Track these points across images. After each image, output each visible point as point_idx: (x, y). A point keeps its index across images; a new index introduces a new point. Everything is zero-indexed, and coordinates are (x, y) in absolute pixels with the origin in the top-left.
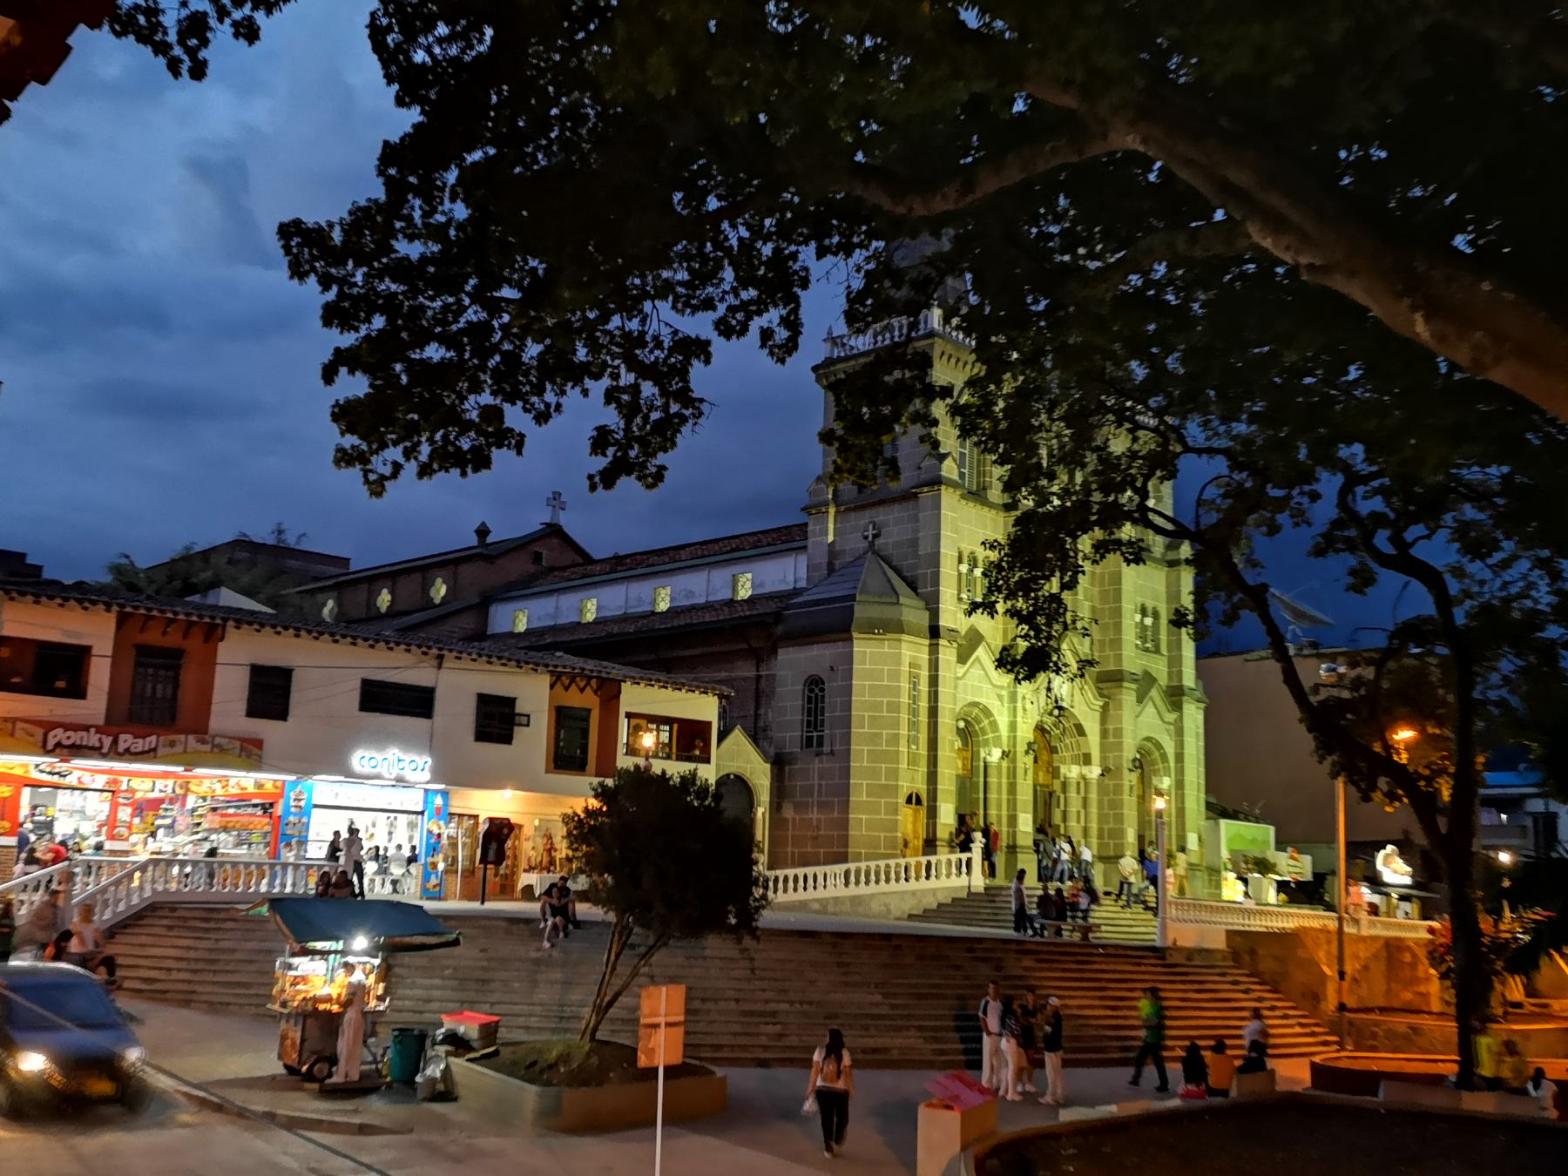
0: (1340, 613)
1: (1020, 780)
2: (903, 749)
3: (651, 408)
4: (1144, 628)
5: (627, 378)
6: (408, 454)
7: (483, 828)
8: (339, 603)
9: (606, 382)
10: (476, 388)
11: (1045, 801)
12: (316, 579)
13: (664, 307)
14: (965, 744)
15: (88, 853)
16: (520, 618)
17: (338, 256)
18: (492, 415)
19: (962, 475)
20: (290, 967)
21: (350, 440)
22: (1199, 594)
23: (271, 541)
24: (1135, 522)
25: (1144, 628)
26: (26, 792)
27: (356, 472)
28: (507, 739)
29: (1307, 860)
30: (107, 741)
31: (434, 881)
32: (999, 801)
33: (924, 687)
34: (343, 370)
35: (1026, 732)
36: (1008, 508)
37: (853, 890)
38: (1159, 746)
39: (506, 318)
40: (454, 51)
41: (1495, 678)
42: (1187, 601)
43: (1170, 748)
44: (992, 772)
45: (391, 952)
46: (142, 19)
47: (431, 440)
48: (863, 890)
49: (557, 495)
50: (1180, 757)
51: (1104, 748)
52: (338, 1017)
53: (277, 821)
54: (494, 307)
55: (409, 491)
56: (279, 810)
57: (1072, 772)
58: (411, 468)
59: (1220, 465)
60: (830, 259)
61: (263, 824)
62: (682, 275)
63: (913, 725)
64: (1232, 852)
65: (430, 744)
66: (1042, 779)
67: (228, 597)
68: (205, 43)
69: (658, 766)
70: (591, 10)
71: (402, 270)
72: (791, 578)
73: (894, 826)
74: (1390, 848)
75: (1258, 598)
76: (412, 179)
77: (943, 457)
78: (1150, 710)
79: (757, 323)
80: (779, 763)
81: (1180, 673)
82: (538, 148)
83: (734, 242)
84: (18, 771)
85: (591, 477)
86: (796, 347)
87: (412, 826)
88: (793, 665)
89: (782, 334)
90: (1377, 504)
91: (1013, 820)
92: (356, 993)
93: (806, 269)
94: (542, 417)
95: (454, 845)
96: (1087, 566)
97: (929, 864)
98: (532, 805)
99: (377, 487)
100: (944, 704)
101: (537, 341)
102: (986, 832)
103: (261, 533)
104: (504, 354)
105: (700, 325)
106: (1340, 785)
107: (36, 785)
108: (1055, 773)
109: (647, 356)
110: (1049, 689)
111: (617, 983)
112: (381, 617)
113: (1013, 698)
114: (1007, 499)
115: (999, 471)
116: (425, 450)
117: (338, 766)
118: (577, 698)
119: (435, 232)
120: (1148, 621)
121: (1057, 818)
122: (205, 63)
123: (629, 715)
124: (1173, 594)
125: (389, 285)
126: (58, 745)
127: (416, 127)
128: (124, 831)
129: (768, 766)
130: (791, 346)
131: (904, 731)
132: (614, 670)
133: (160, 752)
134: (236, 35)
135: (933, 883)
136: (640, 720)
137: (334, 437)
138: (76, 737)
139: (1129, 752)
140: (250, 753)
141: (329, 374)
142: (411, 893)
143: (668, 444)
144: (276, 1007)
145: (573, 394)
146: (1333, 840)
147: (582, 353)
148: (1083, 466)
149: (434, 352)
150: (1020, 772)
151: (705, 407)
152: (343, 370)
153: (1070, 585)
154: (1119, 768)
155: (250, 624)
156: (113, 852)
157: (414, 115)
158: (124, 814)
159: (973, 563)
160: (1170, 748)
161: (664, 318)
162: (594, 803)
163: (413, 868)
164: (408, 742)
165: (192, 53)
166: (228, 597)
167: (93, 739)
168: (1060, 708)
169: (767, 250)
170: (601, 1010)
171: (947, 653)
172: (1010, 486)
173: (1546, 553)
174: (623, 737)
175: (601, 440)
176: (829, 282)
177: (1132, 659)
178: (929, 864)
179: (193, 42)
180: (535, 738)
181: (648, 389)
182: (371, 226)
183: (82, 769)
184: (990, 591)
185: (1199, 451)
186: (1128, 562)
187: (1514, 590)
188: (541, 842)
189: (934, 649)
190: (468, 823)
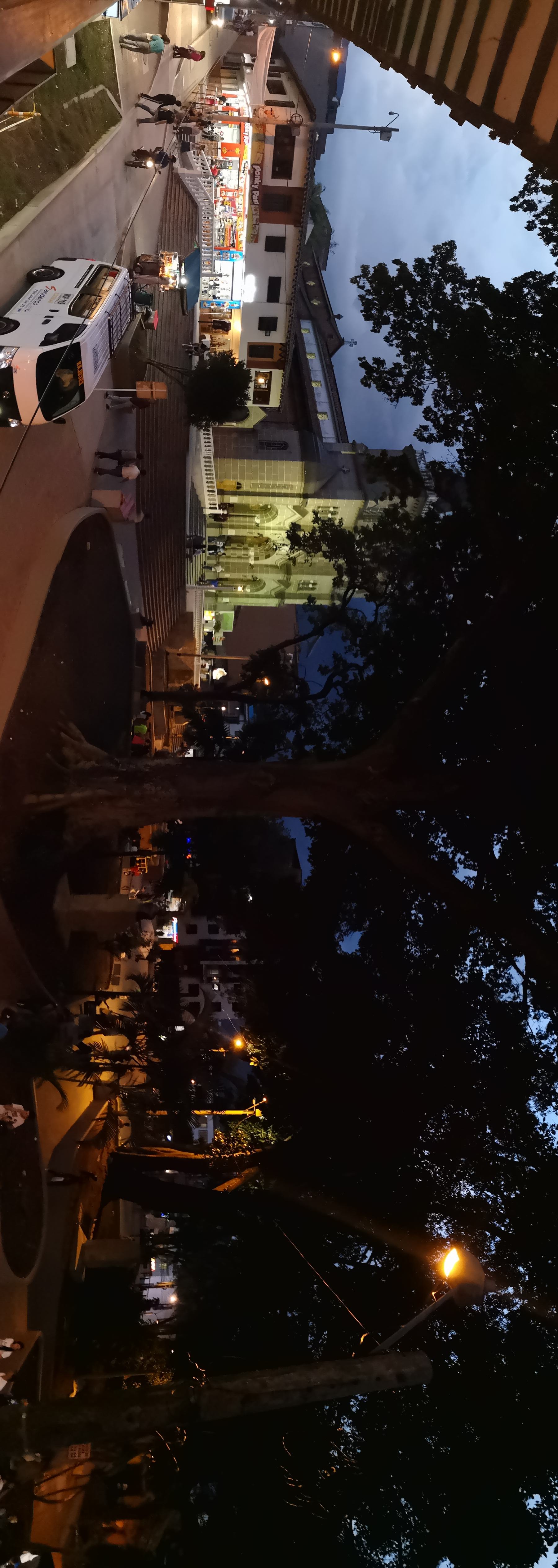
0: (312, 663)
1: (247, 530)
2: (259, 482)
3: (393, 382)
4: (308, 583)
5: (405, 372)
6: (368, 292)
7: (227, 321)
8: (309, 267)
9: (403, 363)
10: (395, 315)
11: (239, 541)
12: (318, 258)
13: (435, 386)
14: (262, 508)
15: (215, 182)
16: (306, 327)
17: (443, 262)
18: (386, 321)
19: (369, 509)
20: (175, 257)
21: (372, 271)
22: (321, 607)
23: (332, 241)
24: (349, 583)
25: (308, 583)
26: (238, 159)
27: (360, 273)
28: (260, 328)
29: (220, 644)
30: (256, 187)
31: (207, 305)
32: (239, 521)
33: (283, 491)
34: (398, 267)
35: (267, 534)
36: (355, 528)
37: (202, 460)
38: (262, 588)
39: (425, 325)
40: (530, 302)
41: (287, 711)
42: (319, 602)
43: (261, 592)
44: (251, 519)
45: (182, 291)
46: (533, 186)
47: (374, 299)
48: (203, 464)
49: (356, 343)
50: (258, 596)
51: (261, 566)
52: (157, 275)
53: (228, 249)
54: (429, 320)
55: (354, 292)
56: (232, 250)
57: (252, 553)
58: (363, 293)
59: (371, 619)
60: (457, 455)
61: (227, 243)
62: (448, 393)
63: (268, 486)
64: (222, 615)
65: (257, 302)
66: (249, 539)
67: (310, 228)
68: (525, 210)
69: (251, 385)
70: (555, 355)
71: (440, 287)
72: (326, 436)
73: (228, 477)
74: (226, 673)
75: (318, 631)
76: (476, 289)
77: (377, 502)
78: (275, 585)
79: (429, 424)
80: (253, 431)
81: (289, 598)
82: (495, 335)
83: (462, 414)
84: (245, 155)
85: (364, 358)
86: (421, 440)
87: (227, 297)
88: (292, 436)
89: (426, 435)
90: (351, 677)
91: (232, 527)
92: (165, 281)
93: (453, 445)
94: (387, 339)
95: (220, 311)
96: (333, 562)
97: (213, 491)
98: (236, 337)
99: (354, 281)
100: (277, 499)
101: (417, 336)
102: (227, 515)
103: (334, 238)
104: (410, 324)
105: (428, 401)
106: (247, 658)
107: (240, 162)
108: (251, 545)
109: (415, 380)
110: (284, 545)
111: (169, 372)
112: (305, 281)
113: (280, 529)
114: (359, 528)
115: (371, 525)
116: (370, 297)
117: (248, 270)
118: (276, 353)
119: (455, 297)
120: (310, 586)
121: (234, 545)
122: (517, 210)
123: (271, 373)
124: (321, 597)
125: (433, 283)
126: (255, 170)
127: (497, 290)
128: (224, 194)
129: (252, 427)
130: (421, 438)
131: (265, 482)
132: (288, 368)
133: (253, 206)
134: (529, 222)
135: (206, 493)
136: (269, 377)
137: (372, 264)
138: (257, 175)
139: (259, 576)
140: (253, 238)
141: (397, 262)
142: (202, 297)
143: (379, 389)
144: (161, 253)
145: (397, 351)
146: (229, 654)
147: (414, 354)
148: (372, 562)
149: (408, 299)
150: (251, 531)
151: (395, 403)
152: (398, 267)
153: (325, 555)
154: (253, 572)
155: (309, 164)
156: (216, 191)
157: (502, 289)
158: (230, 194)
159: (334, 513)
160: (261, 592)
161: (431, 386)
162: (237, 361)
163: (211, 298)
164: (258, 294)
165: (521, 206)
166: (310, 228)
167: (257, 182)
168: (276, 549)
169: (460, 428)
170: (158, 366)
171: (297, 501)
172: (364, 530)
173: (330, 728)
174: (262, 370)
175: (379, 362)
176: (445, 454)
177: (296, 579)
178: (213, 491)
179: (525, 206)
180: (261, 338)
181: (401, 380)
182: (457, 275)
183: (246, 179)
184: (323, 521)
185: (376, 611)
186: (334, 580)
187: (318, 718)
188: (222, 341)
189: (299, 496)
190: (228, 315)
